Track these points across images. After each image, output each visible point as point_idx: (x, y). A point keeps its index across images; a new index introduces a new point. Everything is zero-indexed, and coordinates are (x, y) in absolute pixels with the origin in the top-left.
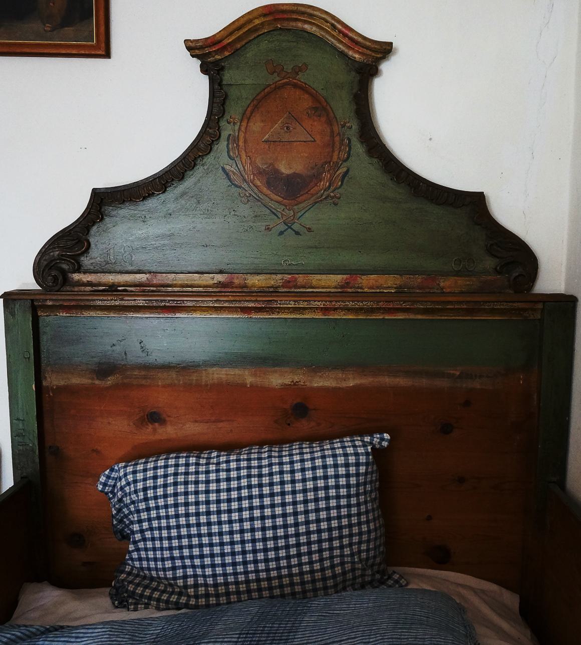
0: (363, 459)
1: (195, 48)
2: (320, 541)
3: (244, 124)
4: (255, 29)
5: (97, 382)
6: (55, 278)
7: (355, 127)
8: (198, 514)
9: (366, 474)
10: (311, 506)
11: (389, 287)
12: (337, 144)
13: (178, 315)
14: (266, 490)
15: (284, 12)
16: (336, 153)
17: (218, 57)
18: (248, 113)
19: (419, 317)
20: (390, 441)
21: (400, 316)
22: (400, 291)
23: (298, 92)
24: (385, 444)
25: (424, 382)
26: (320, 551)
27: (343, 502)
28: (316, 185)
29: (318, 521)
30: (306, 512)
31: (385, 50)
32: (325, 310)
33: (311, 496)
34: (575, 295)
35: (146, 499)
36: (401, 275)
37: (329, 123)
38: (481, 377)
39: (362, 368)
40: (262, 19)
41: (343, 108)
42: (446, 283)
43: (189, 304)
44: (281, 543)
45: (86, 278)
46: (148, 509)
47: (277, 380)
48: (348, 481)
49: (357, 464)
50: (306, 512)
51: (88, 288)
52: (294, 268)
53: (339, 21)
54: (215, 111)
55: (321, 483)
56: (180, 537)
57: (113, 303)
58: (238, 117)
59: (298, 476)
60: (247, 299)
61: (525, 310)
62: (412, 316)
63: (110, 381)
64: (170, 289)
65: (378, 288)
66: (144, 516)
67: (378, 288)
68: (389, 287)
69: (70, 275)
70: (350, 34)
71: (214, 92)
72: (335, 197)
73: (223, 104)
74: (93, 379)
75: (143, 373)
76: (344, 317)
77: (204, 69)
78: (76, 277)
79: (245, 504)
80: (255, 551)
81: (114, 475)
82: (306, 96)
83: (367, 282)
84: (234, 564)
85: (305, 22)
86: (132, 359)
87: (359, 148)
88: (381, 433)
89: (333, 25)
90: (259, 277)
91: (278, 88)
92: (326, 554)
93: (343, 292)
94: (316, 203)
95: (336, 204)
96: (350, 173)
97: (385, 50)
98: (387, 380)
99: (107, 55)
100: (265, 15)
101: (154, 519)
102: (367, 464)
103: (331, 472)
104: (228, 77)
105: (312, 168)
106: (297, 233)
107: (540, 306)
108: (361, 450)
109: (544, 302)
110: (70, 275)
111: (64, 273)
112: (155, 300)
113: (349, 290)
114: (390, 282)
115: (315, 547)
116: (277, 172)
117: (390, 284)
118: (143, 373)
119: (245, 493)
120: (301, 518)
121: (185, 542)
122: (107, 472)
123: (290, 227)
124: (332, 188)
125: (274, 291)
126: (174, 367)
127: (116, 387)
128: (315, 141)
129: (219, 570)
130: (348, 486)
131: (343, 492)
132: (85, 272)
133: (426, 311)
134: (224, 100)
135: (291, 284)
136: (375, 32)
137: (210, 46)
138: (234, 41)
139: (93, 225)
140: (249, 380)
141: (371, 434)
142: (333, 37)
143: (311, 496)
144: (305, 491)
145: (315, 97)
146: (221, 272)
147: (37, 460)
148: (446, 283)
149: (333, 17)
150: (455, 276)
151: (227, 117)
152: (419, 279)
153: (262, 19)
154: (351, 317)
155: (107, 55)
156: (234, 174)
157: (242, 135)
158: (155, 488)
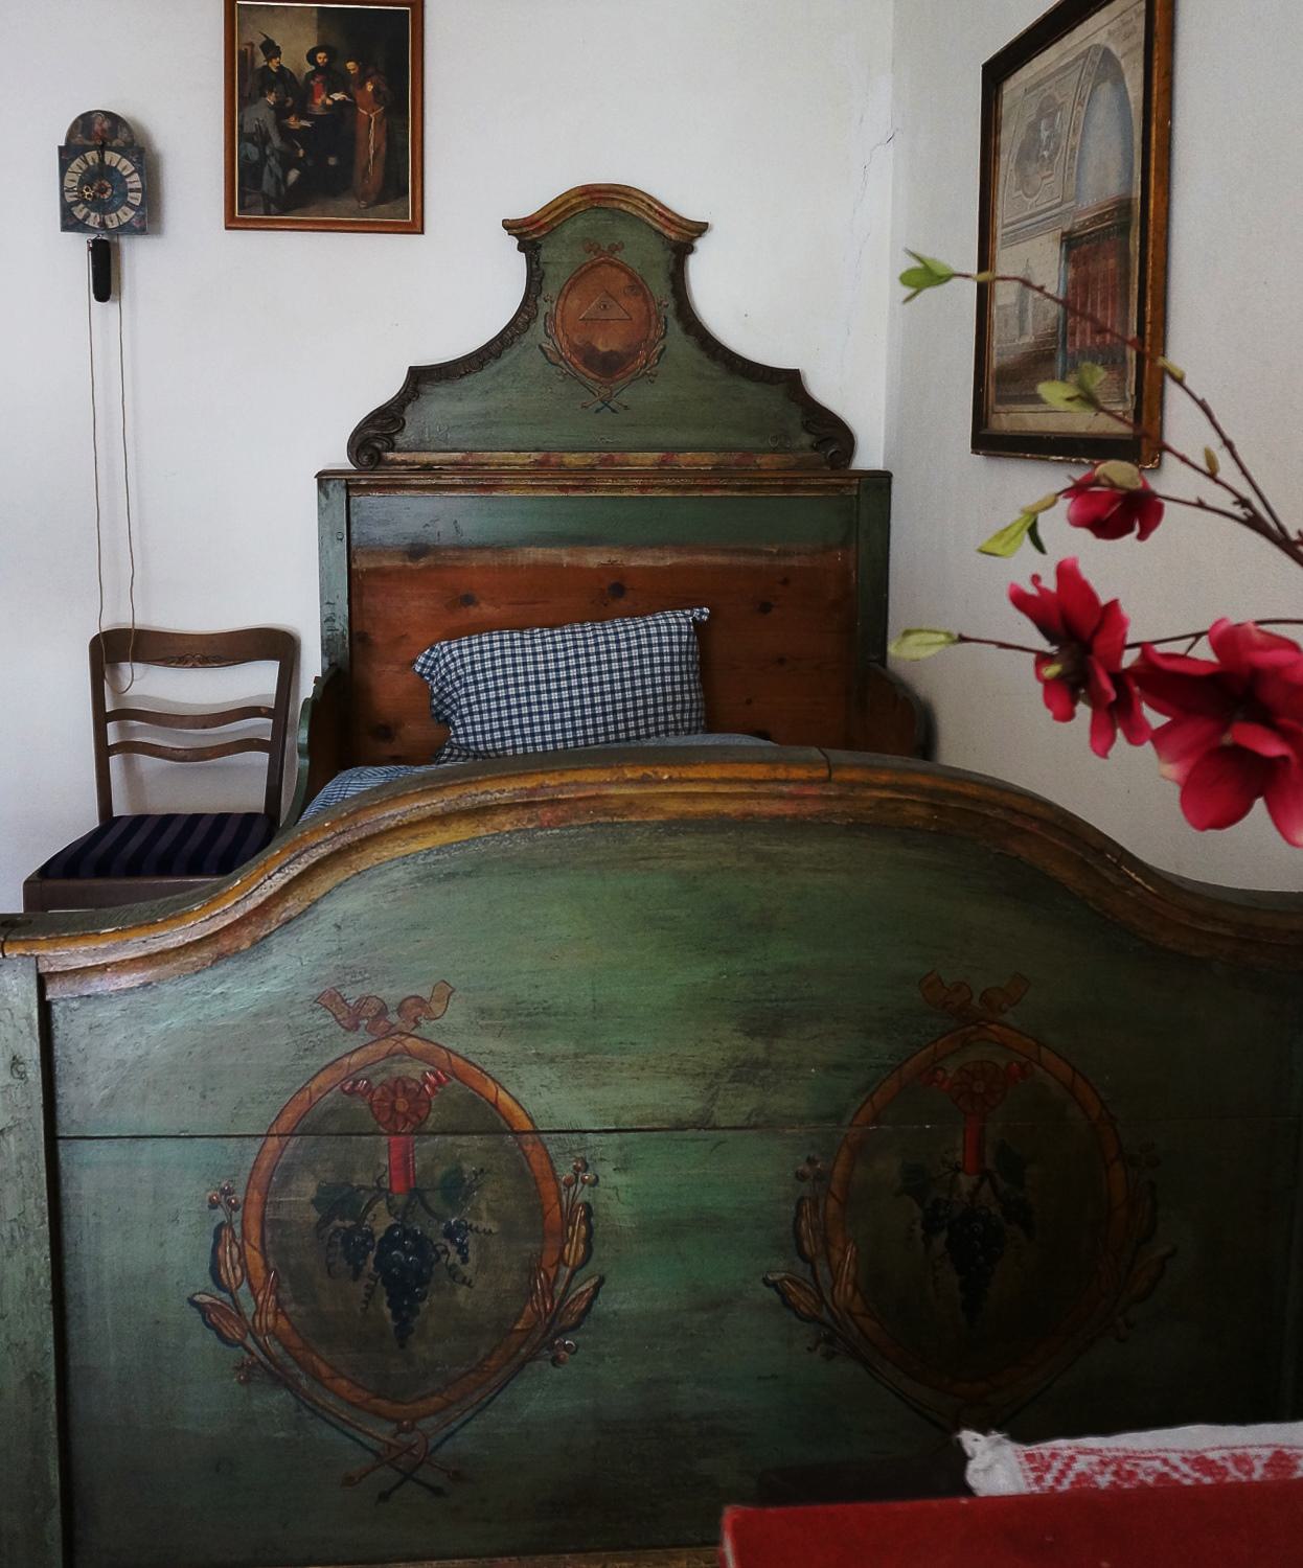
0: (685, 629)
1: (510, 226)
2: (645, 707)
3: (561, 302)
4: (572, 208)
5: (409, 564)
6: (371, 457)
7: (672, 306)
8: (527, 684)
9: (688, 643)
10: (637, 673)
11: (706, 465)
12: (653, 322)
13: (494, 494)
14: (593, 659)
15: (600, 191)
16: (652, 332)
17: (535, 236)
18: (565, 292)
19: (735, 494)
20: (709, 615)
21: (718, 493)
22: (717, 468)
23: (614, 270)
24: (705, 618)
25: (742, 560)
26: (646, 717)
27: (667, 669)
28: (633, 363)
29: (643, 687)
30: (632, 679)
31: (701, 229)
32: (642, 488)
33: (636, 663)
34: (891, 471)
35: (474, 673)
36: (717, 452)
37: (646, 301)
38: (799, 554)
39: (679, 546)
40: (580, 199)
41: (659, 287)
42: (764, 460)
43: (506, 482)
44: (609, 708)
45: (400, 457)
46: (476, 683)
47: (594, 559)
48: (671, 649)
49: (680, 633)
50: (632, 679)
51: (404, 467)
52: (610, 446)
53: (656, 202)
54: (532, 290)
55: (645, 651)
56: (509, 707)
57: (429, 482)
58: (555, 296)
59: (623, 645)
60: (568, 476)
61: (842, 486)
62: (729, 494)
63: (422, 563)
64: (486, 468)
65: (695, 465)
66: (472, 689)
67: (695, 465)
68: (706, 465)
69: (384, 454)
70: (667, 214)
71: (532, 272)
72: (651, 374)
73: (540, 282)
74: (404, 561)
75: (457, 554)
76: (663, 495)
77: (521, 248)
78: (390, 455)
79: (573, 672)
80: (583, 717)
81: (434, 655)
82: (623, 275)
83: (684, 459)
84: (564, 730)
85: (622, 201)
86: (445, 540)
87: (675, 327)
88: (700, 607)
89: (649, 205)
90: (576, 455)
91: (594, 266)
92: (651, 720)
93: (662, 469)
94: (633, 380)
95: (652, 382)
96: (667, 350)
97: (701, 229)
98: (705, 559)
99: (422, 233)
100: (582, 195)
101: (482, 692)
102: (689, 634)
103: (655, 640)
104: (545, 254)
105: (629, 346)
106: (614, 411)
107: (856, 481)
108: (682, 620)
109: (860, 478)
110: (384, 454)
111: (379, 452)
112: (472, 479)
113: (666, 468)
114: (706, 460)
115: (640, 713)
116: (594, 349)
117: (706, 461)
118: (457, 554)
119: (572, 662)
120: (628, 684)
121: (515, 711)
122: (426, 653)
123: (606, 405)
124: (649, 366)
125: (591, 468)
126: (489, 548)
127: (428, 568)
128: (631, 319)
129: (549, 738)
130: (672, 654)
131: (667, 659)
132: (399, 451)
133: (742, 488)
134: (542, 278)
135: (609, 462)
136: (691, 211)
137: (528, 226)
138: (552, 221)
139: (409, 403)
140: (566, 560)
141: (691, 609)
142: (649, 216)
143: (609, 708)
144: (603, 704)
145: (632, 277)
146: (537, 450)
147: (347, 645)
148: (764, 460)
149: (650, 197)
150: (772, 453)
151: (544, 293)
152: (736, 456)
153: (580, 199)
154: (667, 495)
155: (422, 233)
156: (551, 352)
157: (559, 313)
158: (482, 661)
